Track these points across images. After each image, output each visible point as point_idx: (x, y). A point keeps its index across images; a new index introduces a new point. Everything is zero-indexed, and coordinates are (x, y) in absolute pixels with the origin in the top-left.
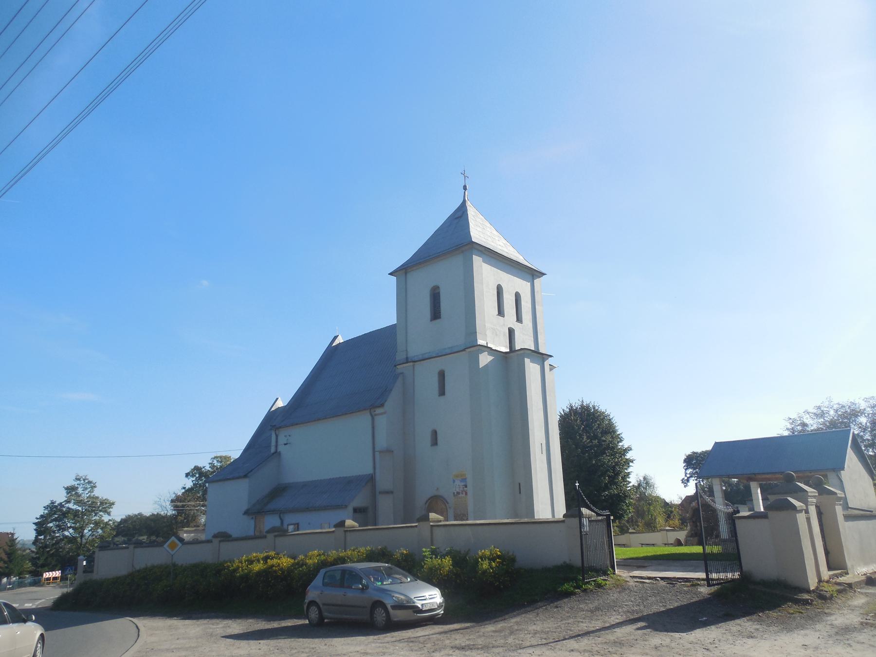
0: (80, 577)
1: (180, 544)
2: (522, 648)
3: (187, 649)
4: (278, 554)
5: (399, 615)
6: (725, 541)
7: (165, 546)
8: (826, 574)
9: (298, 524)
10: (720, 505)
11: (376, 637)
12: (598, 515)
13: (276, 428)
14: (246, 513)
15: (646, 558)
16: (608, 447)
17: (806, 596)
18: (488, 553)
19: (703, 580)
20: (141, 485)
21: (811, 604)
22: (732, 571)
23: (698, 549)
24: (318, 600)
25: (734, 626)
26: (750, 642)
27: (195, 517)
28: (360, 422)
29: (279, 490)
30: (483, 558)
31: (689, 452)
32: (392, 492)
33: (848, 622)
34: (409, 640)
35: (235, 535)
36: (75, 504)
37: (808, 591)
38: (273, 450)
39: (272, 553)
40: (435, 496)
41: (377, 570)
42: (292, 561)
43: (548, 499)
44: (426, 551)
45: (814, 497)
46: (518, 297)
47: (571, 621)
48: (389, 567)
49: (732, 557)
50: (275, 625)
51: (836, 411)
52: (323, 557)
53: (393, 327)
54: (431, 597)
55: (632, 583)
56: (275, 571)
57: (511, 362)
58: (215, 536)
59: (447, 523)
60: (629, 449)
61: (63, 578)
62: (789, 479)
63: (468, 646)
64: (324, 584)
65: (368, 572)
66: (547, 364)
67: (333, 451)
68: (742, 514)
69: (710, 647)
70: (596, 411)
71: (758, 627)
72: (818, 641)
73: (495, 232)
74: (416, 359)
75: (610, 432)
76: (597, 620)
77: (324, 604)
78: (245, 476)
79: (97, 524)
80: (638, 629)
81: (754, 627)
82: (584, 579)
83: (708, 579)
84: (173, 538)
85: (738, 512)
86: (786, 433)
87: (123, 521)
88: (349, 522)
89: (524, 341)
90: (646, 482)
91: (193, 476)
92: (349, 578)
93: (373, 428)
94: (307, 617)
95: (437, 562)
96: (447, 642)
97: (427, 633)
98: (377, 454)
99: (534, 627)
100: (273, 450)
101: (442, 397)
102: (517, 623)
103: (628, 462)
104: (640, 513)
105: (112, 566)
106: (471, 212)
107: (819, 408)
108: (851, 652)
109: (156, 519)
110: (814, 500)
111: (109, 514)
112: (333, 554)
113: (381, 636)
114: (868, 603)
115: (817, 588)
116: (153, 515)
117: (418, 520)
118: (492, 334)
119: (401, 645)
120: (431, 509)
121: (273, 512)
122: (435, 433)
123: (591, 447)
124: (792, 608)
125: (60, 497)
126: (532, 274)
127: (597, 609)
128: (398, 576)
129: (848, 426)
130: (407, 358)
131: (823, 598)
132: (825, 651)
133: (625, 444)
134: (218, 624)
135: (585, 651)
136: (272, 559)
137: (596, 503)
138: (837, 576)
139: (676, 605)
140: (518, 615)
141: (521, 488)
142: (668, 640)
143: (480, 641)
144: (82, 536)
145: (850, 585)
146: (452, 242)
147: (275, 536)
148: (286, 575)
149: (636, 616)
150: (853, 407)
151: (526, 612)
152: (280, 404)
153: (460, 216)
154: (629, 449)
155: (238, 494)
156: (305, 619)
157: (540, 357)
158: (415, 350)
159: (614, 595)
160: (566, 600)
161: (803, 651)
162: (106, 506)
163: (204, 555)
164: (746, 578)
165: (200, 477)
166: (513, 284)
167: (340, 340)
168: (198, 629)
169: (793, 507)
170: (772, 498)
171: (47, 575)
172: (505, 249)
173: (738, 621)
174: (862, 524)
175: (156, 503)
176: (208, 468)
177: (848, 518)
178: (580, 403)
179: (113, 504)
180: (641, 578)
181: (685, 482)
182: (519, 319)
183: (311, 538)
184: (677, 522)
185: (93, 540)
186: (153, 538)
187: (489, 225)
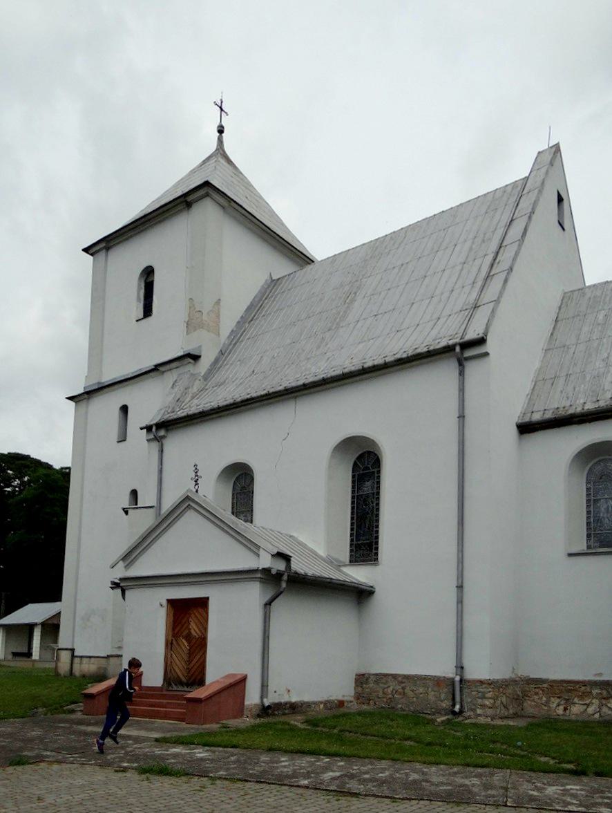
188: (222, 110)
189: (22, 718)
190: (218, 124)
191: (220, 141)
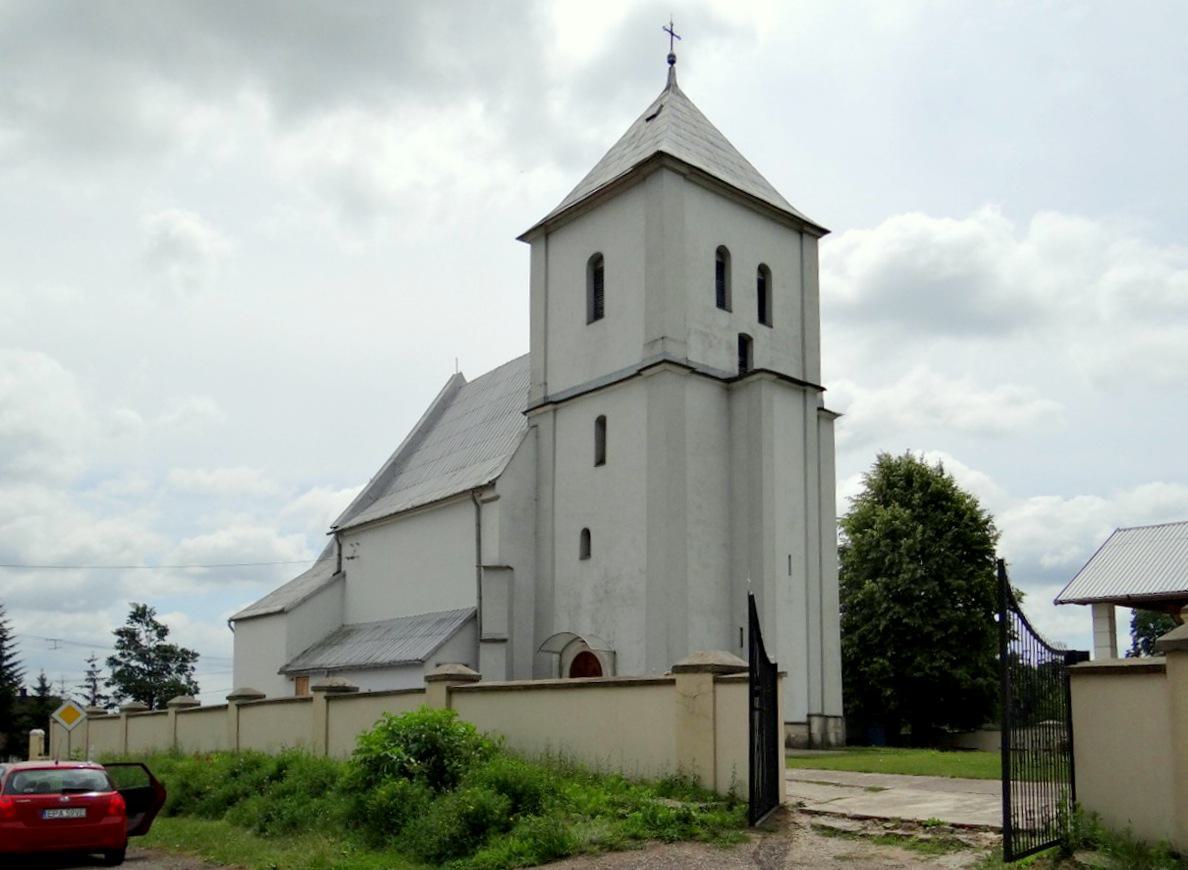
35: (269, 697)
74: (556, 399)
93: (479, 525)
126: (809, 231)
130: (545, 398)
182: (763, 316)
188: (672, 34)
189: (866, 772)
190: (668, 53)
191: (672, 74)
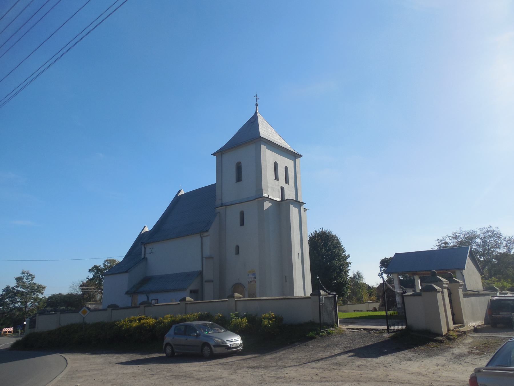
0: (28, 331)
1: (88, 311)
2: (285, 367)
3: (97, 370)
4: (147, 317)
5: (217, 350)
6: (399, 308)
7: (80, 312)
8: (452, 326)
9: (157, 300)
10: (397, 290)
11: (205, 363)
12: (329, 294)
13: (145, 244)
14: (127, 293)
15: (355, 318)
16: (337, 256)
17: (440, 338)
18: (267, 315)
19: (386, 330)
20: (62, 276)
21: (442, 342)
22: (402, 325)
23: (383, 313)
24: (171, 343)
25: (401, 354)
26: (409, 362)
27: (94, 296)
28: (194, 241)
29: (147, 280)
30: (265, 318)
31: (383, 258)
32: (213, 281)
33: (461, 352)
34: (223, 364)
35: (121, 306)
36: (21, 288)
37: (442, 336)
38: (143, 256)
39: (143, 316)
40: (236, 284)
41: (205, 326)
42: (155, 321)
43: (302, 285)
44: (233, 315)
45: (447, 284)
46: (286, 169)
47: (313, 352)
48: (211, 324)
49: (402, 318)
50: (146, 357)
51: (464, 235)
52: (173, 319)
53: (213, 186)
54: (236, 340)
55: (347, 332)
56: (146, 327)
57: (282, 207)
58: (109, 307)
59: (245, 299)
60: (349, 256)
61: (15, 332)
62: (434, 275)
63: (256, 366)
64: (175, 334)
65: (200, 327)
66: (302, 208)
67: (181, 256)
68: (407, 294)
69: (388, 365)
70: (330, 235)
71: (414, 355)
72: (445, 362)
73: (274, 131)
75: (338, 247)
76: (327, 352)
77: (175, 345)
78: (126, 272)
79: (35, 299)
80: (350, 356)
81: (412, 355)
82: (321, 330)
83: (388, 330)
84: (84, 308)
85: (406, 292)
86: (436, 248)
87: (50, 298)
88: (188, 299)
89: (289, 195)
90: (358, 275)
91: (93, 271)
92: (189, 330)
94: (164, 352)
95: (239, 320)
96: (245, 365)
97: (233, 360)
98: (204, 259)
99: (293, 356)
100: (143, 256)
101: (242, 227)
102: (283, 354)
103: (348, 264)
104: (354, 293)
105: (47, 324)
106: (260, 119)
107: (455, 234)
108: (461, 367)
109: (70, 297)
110: (447, 286)
111: (42, 294)
112: (179, 316)
113: (208, 362)
114: (473, 342)
115: (447, 334)
116: (68, 294)
117: (228, 297)
118: (271, 191)
119: (219, 366)
120: (235, 291)
121: (143, 292)
122: (238, 247)
123: (326, 253)
124: (432, 345)
125: (13, 284)
126: (294, 156)
127: (328, 346)
128: (216, 329)
129: (470, 244)
130: (222, 204)
131: (449, 339)
132: (447, 367)
133: (346, 253)
134: (112, 357)
135: (320, 368)
136: (143, 319)
137: (329, 288)
138: (458, 327)
139: (371, 343)
140: (285, 349)
141: (287, 279)
142: (365, 362)
143: (263, 364)
144: (26, 307)
145: (465, 332)
146: (248, 137)
147: (145, 307)
148: (152, 328)
149: (349, 349)
150: (473, 233)
151: (288, 348)
152: (147, 229)
153: (253, 122)
154: (349, 256)
155: (123, 282)
156: (163, 353)
157: (299, 204)
158: (227, 199)
159: (337, 339)
160: (310, 341)
161: (436, 367)
162: (41, 289)
163: (102, 317)
164: (409, 329)
165: (97, 272)
166: (284, 162)
167: (183, 192)
168: (101, 360)
169: (435, 290)
170: (424, 285)
171: (5, 330)
172: (279, 141)
173: (403, 352)
174: (473, 299)
175: (71, 287)
176: (102, 266)
177: (465, 296)
178: (321, 230)
179: (45, 288)
180: (352, 329)
181: (380, 275)
182: (287, 182)
183: (166, 307)
184: (374, 298)
185: (33, 309)
186: (69, 308)
187: (270, 127)
